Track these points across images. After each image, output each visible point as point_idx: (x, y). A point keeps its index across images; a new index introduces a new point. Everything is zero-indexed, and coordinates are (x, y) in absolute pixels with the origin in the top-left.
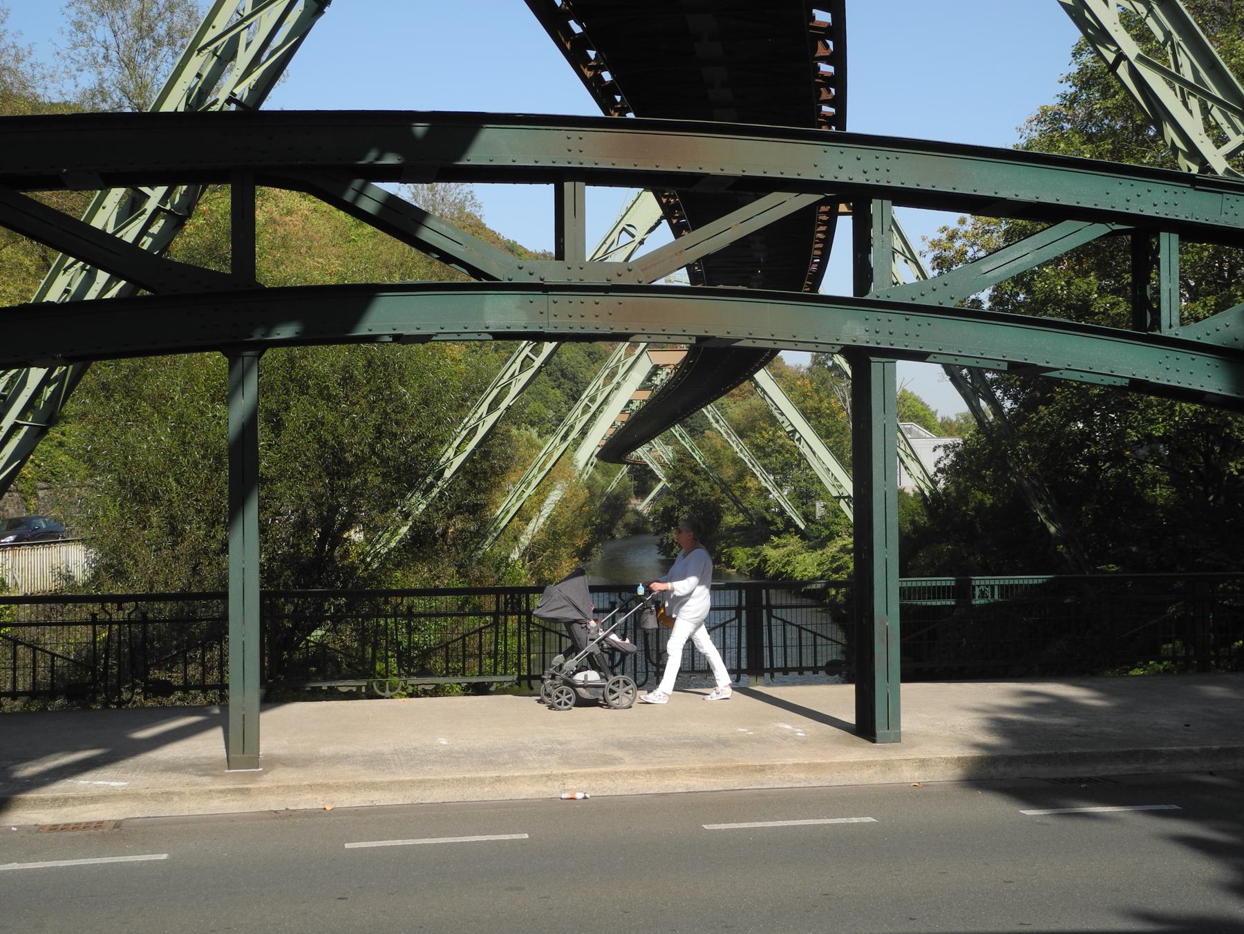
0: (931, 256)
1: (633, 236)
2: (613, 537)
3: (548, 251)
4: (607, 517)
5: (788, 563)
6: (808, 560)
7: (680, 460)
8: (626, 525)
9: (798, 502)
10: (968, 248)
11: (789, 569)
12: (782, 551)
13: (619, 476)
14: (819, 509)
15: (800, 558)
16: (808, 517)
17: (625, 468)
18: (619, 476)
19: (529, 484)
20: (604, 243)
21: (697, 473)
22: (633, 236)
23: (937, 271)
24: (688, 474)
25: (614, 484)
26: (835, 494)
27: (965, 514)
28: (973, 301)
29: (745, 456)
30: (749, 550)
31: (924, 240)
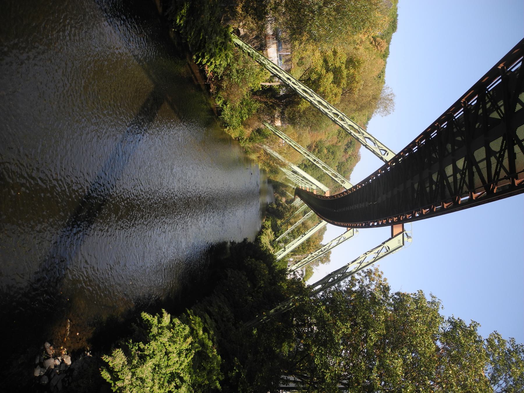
0: (372, 269)
1: (384, 155)
2: (275, 193)
3: (323, 241)
4: (280, 192)
5: (266, 235)
6: (266, 240)
7: (296, 208)
8: (278, 197)
9: (284, 240)
10: (375, 282)
11: (264, 235)
12: (270, 233)
13: (291, 195)
14: (282, 244)
15: (267, 238)
16: (279, 242)
17: (293, 197)
18: (291, 195)
19: (291, 142)
20: (382, 144)
21: (292, 212)
22: (384, 155)
23: (366, 271)
24: (292, 210)
25: (289, 194)
26: (286, 247)
27: (279, 282)
28: (355, 284)
29: (297, 224)
30: (270, 226)
31: (378, 266)
